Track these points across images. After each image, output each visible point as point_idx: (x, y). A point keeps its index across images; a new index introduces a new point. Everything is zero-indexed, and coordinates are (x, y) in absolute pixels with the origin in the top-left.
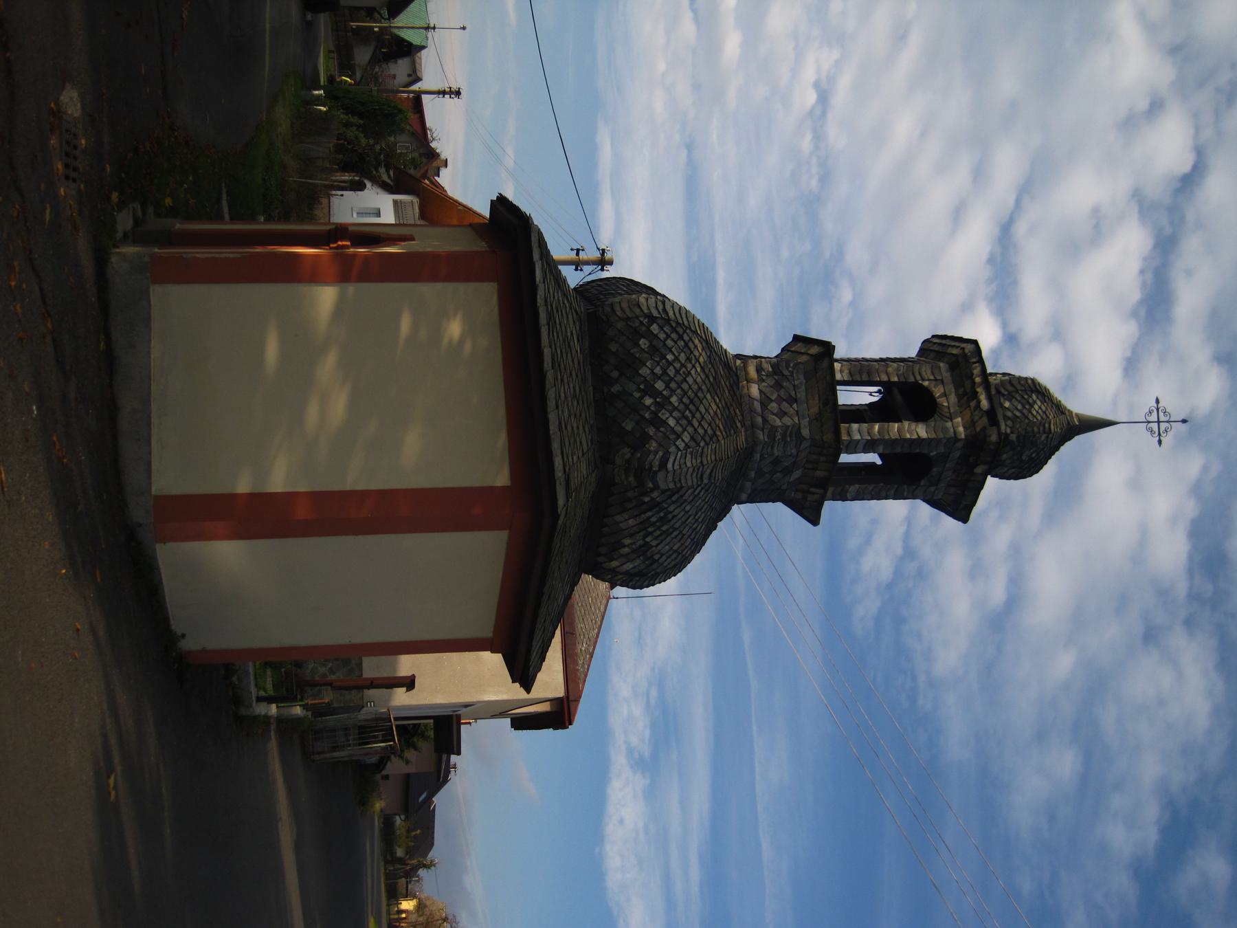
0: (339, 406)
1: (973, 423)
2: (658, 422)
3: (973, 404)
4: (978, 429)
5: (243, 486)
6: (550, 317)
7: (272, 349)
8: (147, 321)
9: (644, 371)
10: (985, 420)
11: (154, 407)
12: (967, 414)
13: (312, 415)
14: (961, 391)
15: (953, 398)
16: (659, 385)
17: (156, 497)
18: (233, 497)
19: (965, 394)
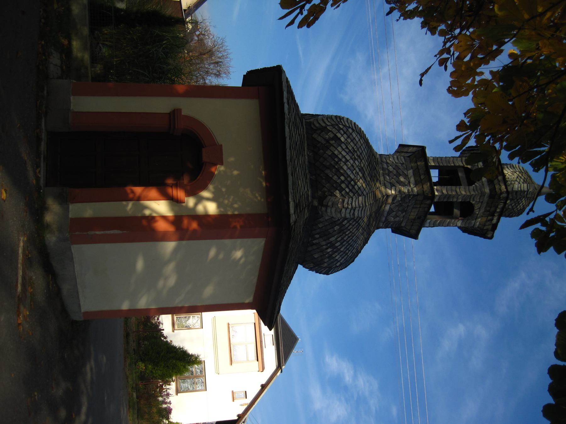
0: (172, 281)
1: (484, 225)
2: (330, 257)
3: (490, 218)
4: (485, 228)
5: (125, 306)
6: (294, 183)
7: (140, 265)
8: (72, 259)
9: (333, 239)
10: (490, 227)
11: (79, 286)
12: (484, 219)
13: (161, 284)
14: (488, 209)
15: (482, 210)
16: (343, 186)
17: (71, 219)
18: (120, 311)
19: (489, 211)
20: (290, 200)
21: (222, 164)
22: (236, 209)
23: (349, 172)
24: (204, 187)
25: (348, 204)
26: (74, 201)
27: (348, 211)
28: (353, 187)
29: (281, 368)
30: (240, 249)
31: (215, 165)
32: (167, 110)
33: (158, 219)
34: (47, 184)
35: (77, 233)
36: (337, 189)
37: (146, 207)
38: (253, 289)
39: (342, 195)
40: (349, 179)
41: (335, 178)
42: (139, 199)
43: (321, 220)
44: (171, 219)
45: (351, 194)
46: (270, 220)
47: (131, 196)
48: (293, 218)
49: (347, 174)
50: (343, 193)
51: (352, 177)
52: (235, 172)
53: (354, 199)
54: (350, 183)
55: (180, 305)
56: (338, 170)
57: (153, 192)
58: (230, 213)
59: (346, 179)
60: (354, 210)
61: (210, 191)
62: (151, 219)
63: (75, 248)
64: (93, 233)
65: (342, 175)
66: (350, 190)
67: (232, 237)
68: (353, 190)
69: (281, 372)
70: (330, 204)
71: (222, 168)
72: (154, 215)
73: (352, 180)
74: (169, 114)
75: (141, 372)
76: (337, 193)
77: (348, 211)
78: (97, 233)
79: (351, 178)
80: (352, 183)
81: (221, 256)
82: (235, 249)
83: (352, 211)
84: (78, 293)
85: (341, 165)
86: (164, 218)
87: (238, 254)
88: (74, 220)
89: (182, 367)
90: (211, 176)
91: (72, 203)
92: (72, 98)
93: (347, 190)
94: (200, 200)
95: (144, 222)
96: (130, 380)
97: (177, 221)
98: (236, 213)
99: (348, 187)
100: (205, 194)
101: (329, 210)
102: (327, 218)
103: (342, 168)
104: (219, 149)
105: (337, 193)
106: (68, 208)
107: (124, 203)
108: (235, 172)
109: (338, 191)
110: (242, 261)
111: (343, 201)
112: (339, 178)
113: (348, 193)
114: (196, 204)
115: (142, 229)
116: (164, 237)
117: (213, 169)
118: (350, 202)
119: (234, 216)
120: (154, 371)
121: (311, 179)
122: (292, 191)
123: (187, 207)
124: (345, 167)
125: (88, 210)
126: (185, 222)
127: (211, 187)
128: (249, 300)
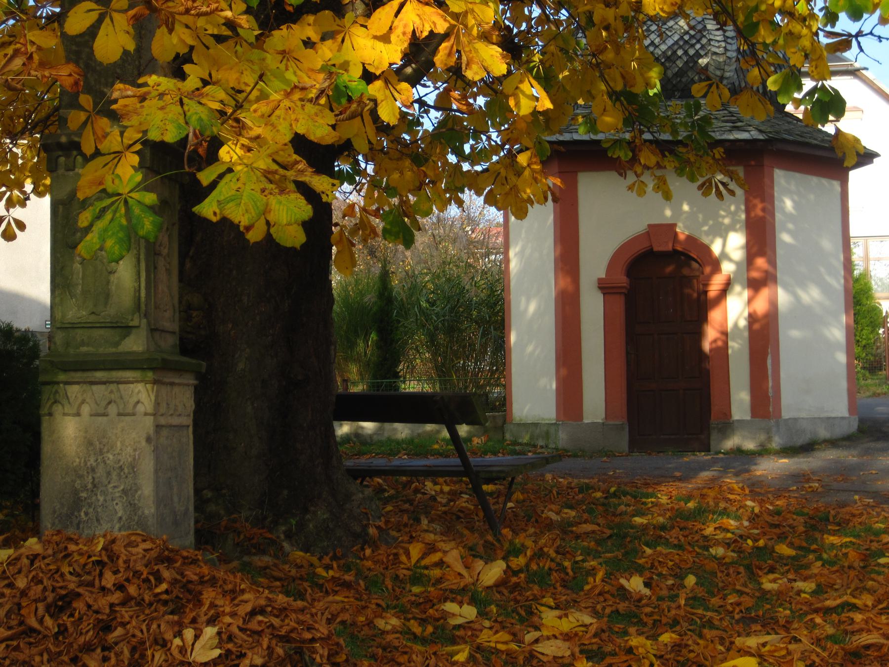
5: (842, 358)
16: (692, 52)
17: (752, 417)
20: (731, 137)
21: (674, 226)
22: (738, 208)
23: (670, 42)
24: (707, 250)
25: (719, 47)
26: (728, 414)
27: (729, 47)
28: (692, 37)
29: (858, 70)
30: (784, 202)
31: (676, 234)
32: (599, 298)
33: (751, 310)
34: (707, 449)
35: (771, 410)
36: (697, 62)
37: (736, 325)
38: (825, 181)
39: (706, 55)
40: (681, 43)
41: (680, 64)
42: (725, 334)
43: (737, 84)
44: (751, 292)
45: (704, 41)
46: (753, 163)
47: (720, 343)
48: (755, 134)
49: (673, 45)
50: (702, 53)
51: (676, 37)
52: (686, 207)
53: (711, 37)
54: (686, 42)
55: (842, 281)
56: (668, 59)
57: (715, 315)
58: (743, 216)
59: (680, 47)
60: (728, 37)
61: (712, 242)
62: (752, 318)
63: (786, 414)
64: (770, 390)
65: (675, 52)
66: (698, 41)
67: (773, 216)
68: (698, 38)
69: (866, 69)
70: (718, 73)
71: (680, 225)
72: (746, 314)
73: (682, 38)
74: (604, 294)
75: (864, 368)
76: (703, 61)
77: (729, 47)
78: (770, 384)
79: (678, 40)
80: (686, 37)
81: (790, 226)
82: (783, 209)
83: (729, 41)
84: (829, 418)
85: (660, 53)
86: (750, 301)
87: (789, 204)
88: (754, 413)
89: (858, 286)
90: (691, 239)
91: (731, 416)
92: (586, 421)
93: (698, 46)
94: (724, 255)
95: (756, 326)
96: (879, 391)
97: (755, 285)
98: (743, 207)
99: (693, 46)
100: (716, 248)
101: (727, 74)
102: (736, 76)
103: (664, 53)
104: (655, 230)
105: (703, 61)
106: (738, 421)
107: (730, 351)
108: (686, 207)
109: (700, 61)
110: (796, 198)
111: (715, 53)
112: (680, 57)
113: (703, 47)
114: (730, 260)
115: (763, 332)
116: (773, 303)
117: (682, 237)
118: (717, 44)
119: (748, 211)
120: (864, 342)
121: (679, 97)
122: (718, 134)
123: (736, 273)
124: (663, 47)
125: (740, 399)
126: (755, 274)
127: (705, 240)
128: (836, 185)
